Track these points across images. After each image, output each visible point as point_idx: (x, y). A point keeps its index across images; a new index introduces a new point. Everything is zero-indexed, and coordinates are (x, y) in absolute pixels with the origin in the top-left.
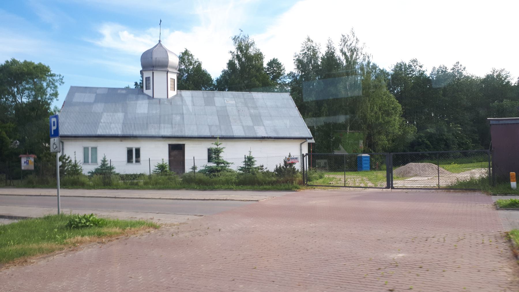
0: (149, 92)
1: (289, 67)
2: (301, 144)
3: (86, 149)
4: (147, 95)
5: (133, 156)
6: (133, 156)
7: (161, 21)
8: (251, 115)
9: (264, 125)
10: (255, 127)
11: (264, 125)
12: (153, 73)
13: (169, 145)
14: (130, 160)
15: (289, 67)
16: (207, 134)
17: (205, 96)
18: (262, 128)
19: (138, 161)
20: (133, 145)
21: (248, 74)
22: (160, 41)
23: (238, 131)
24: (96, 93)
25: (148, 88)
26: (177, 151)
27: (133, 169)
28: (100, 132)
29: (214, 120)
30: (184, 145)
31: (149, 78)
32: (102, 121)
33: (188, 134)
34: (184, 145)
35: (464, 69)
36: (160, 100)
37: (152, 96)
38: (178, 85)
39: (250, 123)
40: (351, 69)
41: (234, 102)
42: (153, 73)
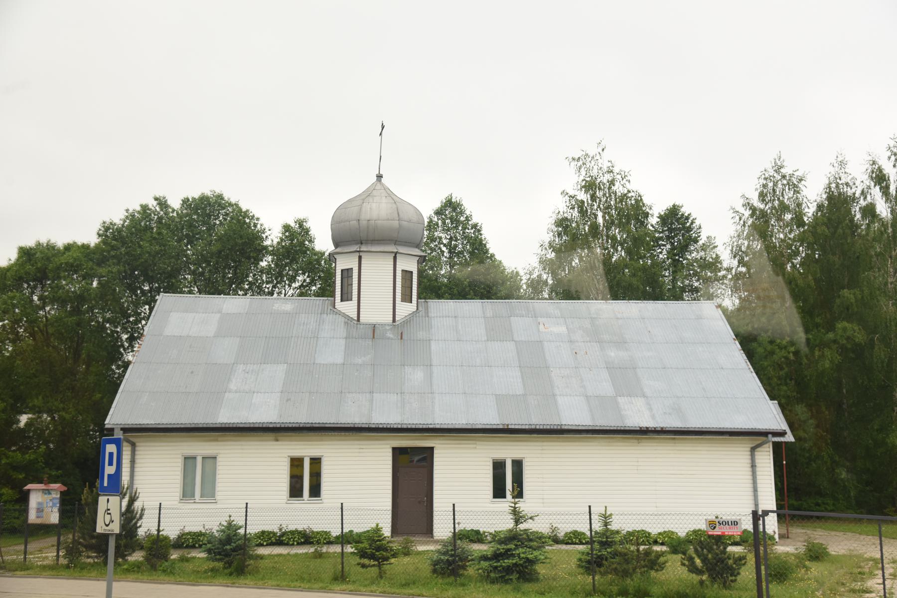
0: (348, 308)
1: (720, 229)
2: (753, 450)
3: (189, 461)
4: (345, 316)
5: (305, 481)
6: (305, 481)
7: (383, 128)
8: (610, 368)
9: (644, 396)
10: (621, 400)
11: (644, 396)
12: (360, 258)
13: (394, 449)
14: (295, 491)
15: (720, 229)
16: (490, 418)
17: (489, 313)
18: (640, 402)
19: (316, 491)
20: (306, 449)
21: (630, 252)
22: (379, 177)
23: (574, 414)
24: (220, 312)
25: (346, 297)
26: (413, 470)
27: (307, 516)
28: (224, 417)
29: (510, 381)
30: (432, 449)
31: (349, 271)
32: (232, 386)
33: (441, 419)
34: (432, 449)
35: (889, 158)
36: (374, 327)
37: (355, 317)
38: (418, 287)
39: (606, 388)
40: (113, 248)
41: (562, 329)
42: (360, 258)
